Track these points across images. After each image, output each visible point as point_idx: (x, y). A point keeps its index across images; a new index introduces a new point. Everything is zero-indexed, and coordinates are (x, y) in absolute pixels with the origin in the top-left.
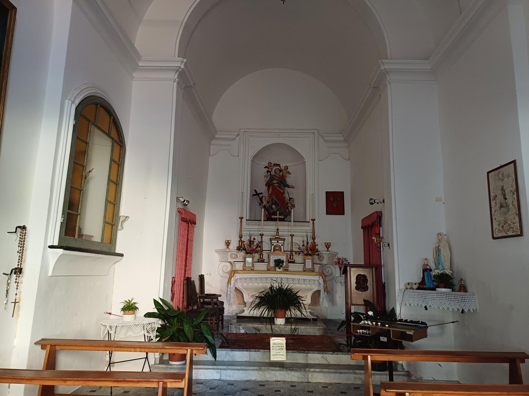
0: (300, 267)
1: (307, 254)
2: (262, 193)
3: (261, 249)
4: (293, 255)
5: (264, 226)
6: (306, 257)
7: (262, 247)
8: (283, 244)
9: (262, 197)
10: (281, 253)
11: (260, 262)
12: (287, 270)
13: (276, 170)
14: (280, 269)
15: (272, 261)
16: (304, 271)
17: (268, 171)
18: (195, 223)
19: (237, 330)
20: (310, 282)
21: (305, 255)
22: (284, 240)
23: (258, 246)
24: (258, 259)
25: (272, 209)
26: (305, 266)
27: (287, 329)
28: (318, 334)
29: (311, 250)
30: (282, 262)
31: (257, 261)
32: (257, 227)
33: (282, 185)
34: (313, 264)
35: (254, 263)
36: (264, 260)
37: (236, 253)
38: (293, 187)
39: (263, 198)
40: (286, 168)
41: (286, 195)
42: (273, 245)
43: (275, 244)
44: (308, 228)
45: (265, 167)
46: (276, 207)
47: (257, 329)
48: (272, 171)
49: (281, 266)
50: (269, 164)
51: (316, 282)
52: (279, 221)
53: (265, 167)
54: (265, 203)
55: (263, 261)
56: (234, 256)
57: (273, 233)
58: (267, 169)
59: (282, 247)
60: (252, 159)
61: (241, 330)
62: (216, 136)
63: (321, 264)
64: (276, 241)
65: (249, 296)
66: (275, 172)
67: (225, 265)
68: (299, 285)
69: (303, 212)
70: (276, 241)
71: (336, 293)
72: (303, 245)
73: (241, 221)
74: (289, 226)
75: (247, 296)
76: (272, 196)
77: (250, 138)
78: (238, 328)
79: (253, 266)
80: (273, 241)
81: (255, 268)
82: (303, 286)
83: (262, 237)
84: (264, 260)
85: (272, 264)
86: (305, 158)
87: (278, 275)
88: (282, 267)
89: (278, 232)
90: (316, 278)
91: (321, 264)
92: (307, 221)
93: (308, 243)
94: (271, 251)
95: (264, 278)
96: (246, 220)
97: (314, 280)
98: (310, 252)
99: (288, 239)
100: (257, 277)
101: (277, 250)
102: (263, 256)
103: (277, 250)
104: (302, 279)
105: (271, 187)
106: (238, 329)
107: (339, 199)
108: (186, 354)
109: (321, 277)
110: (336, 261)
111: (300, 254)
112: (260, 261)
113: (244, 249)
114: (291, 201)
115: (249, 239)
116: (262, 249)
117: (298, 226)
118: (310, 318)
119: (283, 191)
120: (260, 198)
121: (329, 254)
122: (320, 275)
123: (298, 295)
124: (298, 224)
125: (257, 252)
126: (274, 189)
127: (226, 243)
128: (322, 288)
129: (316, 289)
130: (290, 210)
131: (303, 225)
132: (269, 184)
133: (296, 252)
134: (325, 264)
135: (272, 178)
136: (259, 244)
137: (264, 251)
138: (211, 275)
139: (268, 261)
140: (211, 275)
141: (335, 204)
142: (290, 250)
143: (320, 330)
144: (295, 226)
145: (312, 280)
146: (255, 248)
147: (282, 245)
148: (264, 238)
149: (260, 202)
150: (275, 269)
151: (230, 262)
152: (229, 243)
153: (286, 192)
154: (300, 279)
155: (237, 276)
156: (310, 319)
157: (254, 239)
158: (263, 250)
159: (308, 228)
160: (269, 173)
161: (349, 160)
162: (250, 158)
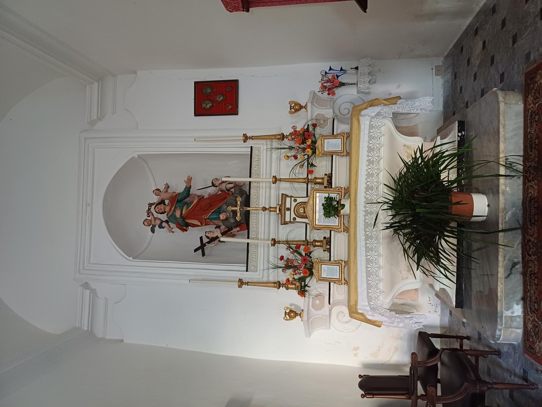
1: (311, 149)
2: (201, 238)
3: (303, 245)
4: (315, 178)
6: (319, 150)
7: (299, 243)
8: (293, 199)
9: (208, 237)
10: (311, 202)
11: (330, 245)
12: (347, 191)
13: (158, 212)
14: (344, 206)
16: (348, 154)
17: (161, 227)
19: (515, 324)
20: (374, 138)
21: (314, 152)
22: (284, 196)
23: (296, 251)
24: (324, 251)
25: (227, 219)
26: (337, 153)
27: (508, 189)
28: (520, 107)
29: (304, 142)
30: (329, 200)
31: (327, 254)
33: (187, 200)
34: (333, 135)
35: (332, 259)
36: (325, 238)
37: (311, 299)
38: (188, 179)
41: (206, 193)
42: (294, 219)
43: (293, 215)
44: (261, 147)
45: (153, 231)
47: (511, 269)
49: (338, 202)
51: (376, 122)
52: (249, 207)
53: (153, 231)
55: (328, 241)
56: (317, 302)
57: (272, 218)
58: (157, 228)
59: (299, 200)
60: (131, 258)
61: (513, 313)
62: (86, 329)
63: (334, 119)
64: (288, 213)
65: (407, 278)
66: (161, 213)
67: (337, 316)
68: (382, 162)
70: (288, 213)
71: (390, 94)
72: (296, 157)
73: (247, 283)
74: (258, 188)
75: (407, 281)
77: (91, 262)
78: (509, 322)
81: (344, 257)
82: (383, 152)
84: (325, 238)
85: (334, 221)
88: (341, 200)
89: (270, 209)
90: (365, 122)
91: (334, 119)
92: (250, 153)
93: (291, 148)
94: (306, 224)
95: (366, 244)
96: (247, 271)
97: (371, 127)
98: (309, 142)
99: (285, 188)
100: (364, 258)
101: (304, 212)
102: (317, 239)
103: (304, 212)
104: (368, 156)
106: (512, 321)
107: (209, 91)
108: (293, 156)
109: (363, 113)
110: (328, 92)
111: (312, 163)
112: (328, 247)
114: (217, 184)
115: (281, 269)
116: (304, 241)
118: (458, 136)
120: (208, 243)
122: (359, 114)
123: (409, 160)
124: (256, 168)
125: (309, 254)
126: (192, 214)
127: (291, 318)
128: (389, 110)
129: (389, 124)
131: (256, 159)
132: (184, 226)
133: (310, 172)
135: (171, 219)
137: (308, 238)
141: (218, 99)
142: (305, 185)
143: (508, 102)
144: (258, 175)
146: (300, 258)
147: (295, 201)
152: (291, 311)
153: (199, 193)
154: (368, 161)
155: (363, 306)
156: (460, 137)
157: (282, 258)
158: (305, 240)
159: (261, 147)
160: (164, 224)
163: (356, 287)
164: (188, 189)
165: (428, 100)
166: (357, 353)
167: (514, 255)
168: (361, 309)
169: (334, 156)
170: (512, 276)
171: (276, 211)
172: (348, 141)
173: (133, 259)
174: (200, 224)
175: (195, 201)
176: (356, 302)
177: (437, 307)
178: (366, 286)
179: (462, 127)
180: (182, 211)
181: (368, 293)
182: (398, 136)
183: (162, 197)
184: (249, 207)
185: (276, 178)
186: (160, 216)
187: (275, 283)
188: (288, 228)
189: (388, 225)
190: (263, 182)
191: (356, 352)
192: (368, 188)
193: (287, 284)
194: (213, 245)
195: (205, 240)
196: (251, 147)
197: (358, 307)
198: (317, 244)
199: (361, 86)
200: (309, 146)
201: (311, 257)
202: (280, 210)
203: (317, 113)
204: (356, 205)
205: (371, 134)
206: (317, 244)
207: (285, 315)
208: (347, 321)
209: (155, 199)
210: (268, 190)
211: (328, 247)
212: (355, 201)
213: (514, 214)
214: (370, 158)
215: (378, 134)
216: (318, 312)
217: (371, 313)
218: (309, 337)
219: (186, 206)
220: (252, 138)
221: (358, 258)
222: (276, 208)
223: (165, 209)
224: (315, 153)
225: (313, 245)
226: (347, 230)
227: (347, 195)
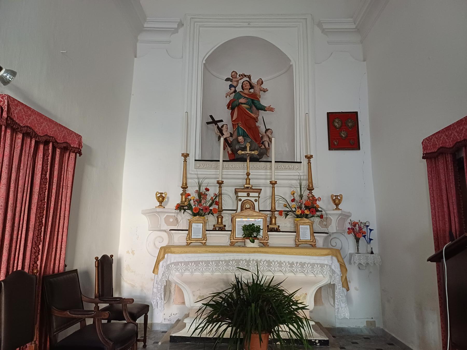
0: (289, 239)
3: (219, 208)
4: (276, 218)
5: (223, 171)
6: (300, 220)
7: (220, 204)
8: (257, 198)
9: (222, 126)
10: (255, 214)
11: (219, 230)
12: (265, 245)
13: (243, 84)
14: (253, 242)
15: (238, 229)
16: (297, 246)
17: (231, 86)
18: (78, 151)
21: (298, 216)
22: (259, 191)
23: (213, 202)
24: (214, 225)
25: (239, 142)
26: (298, 236)
29: (307, 207)
30: (258, 230)
31: (212, 228)
32: (212, 172)
33: (254, 108)
34: (313, 233)
35: (207, 232)
36: (225, 226)
37: (174, 215)
39: (224, 129)
40: (261, 82)
41: (260, 124)
42: (240, 200)
43: (243, 199)
45: (227, 80)
46: (245, 140)
48: (237, 85)
49: (256, 237)
50: (234, 73)
51: (326, 269)
52: (250, 161)
53: (227, 80)
54: (226, 135)
55: (222, 229)
56: (171, 220)
58: (230, 83)
59: (256, 204)
60: (204, 62)
64: (245, 194)
65: (194, 295)
66: (242, 86)
67: (160, 237)
69: (288, 150)
70: (245, 194)
72: (293, 200)
73: (185, 161)
74: (266, 169)
75: (191, 295)
76: (238, 124)
79: (205, 237)
80: (240, 194)
81: (209, 242)
82: (300, 276)
83: (220, 187)
84: (225, 226)
85: (239, 234)
86: (291, 59)
87: (250, 254)
89: (248, 179)
92: (296, 161)
93: (301, 196)
94: (236, 210)
95: (222, 261)
96: (195, 160)
97: (322, 266)
98: (307, 212)
99: (266, 192)
100: (210, 259)
101: (246, 209)
102: (224, 220)
103: (246, 209)
104: (297, 263)
105: (236, 110)
107: (350, 124)
109: (335, 258)
111: (288, 215)
112: (217, 229)
113: (190, 207)
114: (267, 133)
115: (198, 189)
117: (281, 169)
118: (316, 340)
119: (256, 116)
120: (218, 127)
121: (341, 214)
124: (282, 166)
125: (211, 212)
126: (242, 113)
129: (325, 281)
130: (267, 146)
132: (232, 106)
133: (281, 213)
134: (332, 233)
135: (238, 95)
136: (215, 198)
137: (224, 212)
138: (133, 254)
139: (232, 228)
140: (133, 254)
144: (277, 169)
145: (317, 264)
146: (208, 205)
148: (224, 189)
149: (219, 133)
150: (245, 242)
151: (165, 231)
152: (163, 198)
153: (260, 118)
154: (293, 263)
155: (171, 258)
156: (315, 342)
157: (207, 190)
159: (302, 170)
160: (233, 89)
161: (364, 61)
162: (200, 60)
169: (295, 234)
171: (246, 184)
172: (309, 245)
174: (233, 119)
175: (253, 115)
178: (187, 260)
180: (244, 104)
181: (181, 262)
183: (256, 86)
184: (250, 161)
185: (275, 184)
186: (240, 85)
187: (186, 184)
191: (130, 252)
193: (185, 194)
195: (220, 124)
197: (169, 254)
198: (220, 219)
199: (356, 257)
200: (303, 212)
202: (248, 187)
204: (254, 252)
206: (220, 219)
207: (160, 193)
209: (254, 81)
210: (264, 177)
211: (217, 229)
212: (258, 252)
214: (295, 264)
215: (316, 272)
217: (165, 265)
220: (309, 163)
221: (210, 255)
222: (249, 184)
223: (246, 89)
224: (297, 217)
225: (219, 216)
226: (232, 245)
227: (261, 244)
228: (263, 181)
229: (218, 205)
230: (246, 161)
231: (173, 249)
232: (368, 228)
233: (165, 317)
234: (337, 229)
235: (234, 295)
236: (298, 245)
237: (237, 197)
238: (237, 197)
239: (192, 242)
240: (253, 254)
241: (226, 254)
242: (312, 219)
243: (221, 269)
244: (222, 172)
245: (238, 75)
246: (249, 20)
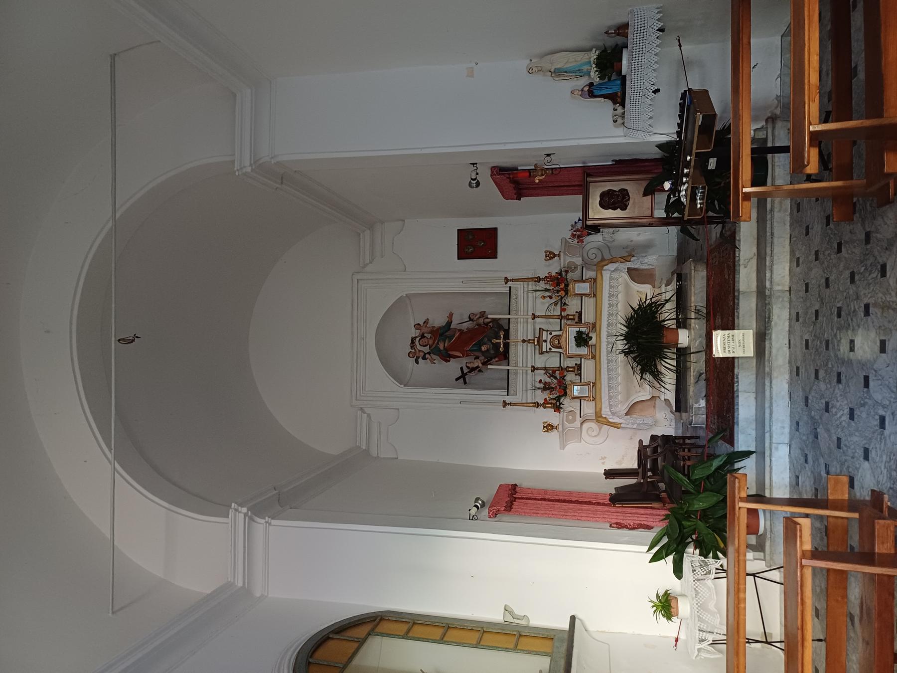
0: (589, 303)
1: (564, 291)
2: (462, 368)
3: (558, 370)
5: (518, 365)
6: (570, 292)
8: (549, 332)
9: (468, 367)
10: (564, 335)
12: (593, 326)
14: (591, 337)
16: (595, 296)
17: (424, 358)
19: (701, 412)
20: (613, 287)
21: (567, 294)
22: (541, 330)
23: (552, 376)
24: (576, 375)
25: (488, 350)
26: (586, 295)
29: (558, 284)
30: (580, 333)
34: (582, 280)
35: (582, 381)
36: (576, 364)
37: (565, 414)
39: (470, 365)
40: (417, 326)
41: (465, 327)
42: (550, 349)
43: (549, 346)
45: (417, 362)
46: (486, 344)
49: (587, 335)
50: (411, 355)
51: (615, 275)
53: (417, 362)
54: (478, 363)
55: (579, 367)
57: (529, 348)
58: (420, 360)
59: (554, 333)
60: (402, 386)
61: (700, 405)
62: (364, 448)
64: (544, 344)
65: (640, 392)
66: (424, 346)
70: (544, 344)
72: (551, 297)
73: (510, 404)
74: (517, 323)
75: (640, 394)
77: (367, 390)
81: (592, 320)
83: (538, 369)
85: (584, 351)
89: (528, 341)
90: (606, 275)
93: (546, 290)
94: (560, 353)
95: (608, 366)
96: (508, 395)
97: (611, 279)
98: (563, 286)
99: (540, 323)
100: (606, 377)
101: (559, 343)
103: (559, 343)
105: (451, 353)
106: (699, 410)
107: (471, 237)
109: (605, 268)
111: (565, 303)
114: (475, 319)
116: (558, 367)
118: (677, 285)
120: (470, 372)
121: (565, 253)
124: (514, 306)
126: (454, 347)
132: (446, 357)
133: (563, 310)
134: (583, 261)
135: (435, 351)
136: (549, 374)
137: (562, 365)
144: (517, 311)
146: (556, 381)
149: (476, 371)
151: (582, 424)
153: (459, 327)
154: (609, 304)
155: (606, 412)
156: (678, 285)
157: (540, 381)
158: (559, 366)
159: (519, 288)
160: (427, 356)
161: (404, 221)
162: (400, 390)
163: (601, 397)
164: (449, 323)
165: (654, 258)
166: (604, 462)
167: (701, 368)
168: (603, 414)
169: (583, 297)
170: (699, 382)
172: (594, 284)
173: (404, 386)
175: (457, 335)
176: (601, 409)
177: (671, 421)
178: (608, 397)
179: (679, 278)
180: (444, 343)
181: (609, 402)
182: (632, 285)
183: (423, 331)
187: (534, 403)
188: (544, 357)
189: (621, 351)
190: (521, 318)
191: (603, 461)
192: (609, 325)
193: (544, 405)
194: (474, 374)
195: (466, 370)
196: (510, 287)
197: (602, 413)
198: (569, 369)
199: (606, 236)
201: (565, 380)
203: (568, 261)
204: (600, 337)
205: (611, 284)
206: (569, 369)
208: (596, 434)
209: (415, 333)
210: (525, 325)
211: (579, 372)
213: (700, 342)
214: (610, 302)
216: (571, 425)
217: (611, 417)
218: (564, 449)
219: (447, 339)
221: (602, 377)
222: (534, 340)
223: (428, 342)
224: (568, 294)
225: (566, 370)
226: (594, 357)
227: (594, 329)
228: (530, 326)
229: (556, 371)
230: (509, 343)
231: (598, 410)
232: (577, 222)
233: (668, 425)
234: (578, 257)
235: (633, 356)
236: (594, 294)
237: (547, 352)
238: (547, 352)
239: (592, 396)
240: (602, 339)
241: (602, 363)
242: (568, 280)
243: (615, 367)
244: (520, 367)
245: (412, 351)
246: (359, 339)
